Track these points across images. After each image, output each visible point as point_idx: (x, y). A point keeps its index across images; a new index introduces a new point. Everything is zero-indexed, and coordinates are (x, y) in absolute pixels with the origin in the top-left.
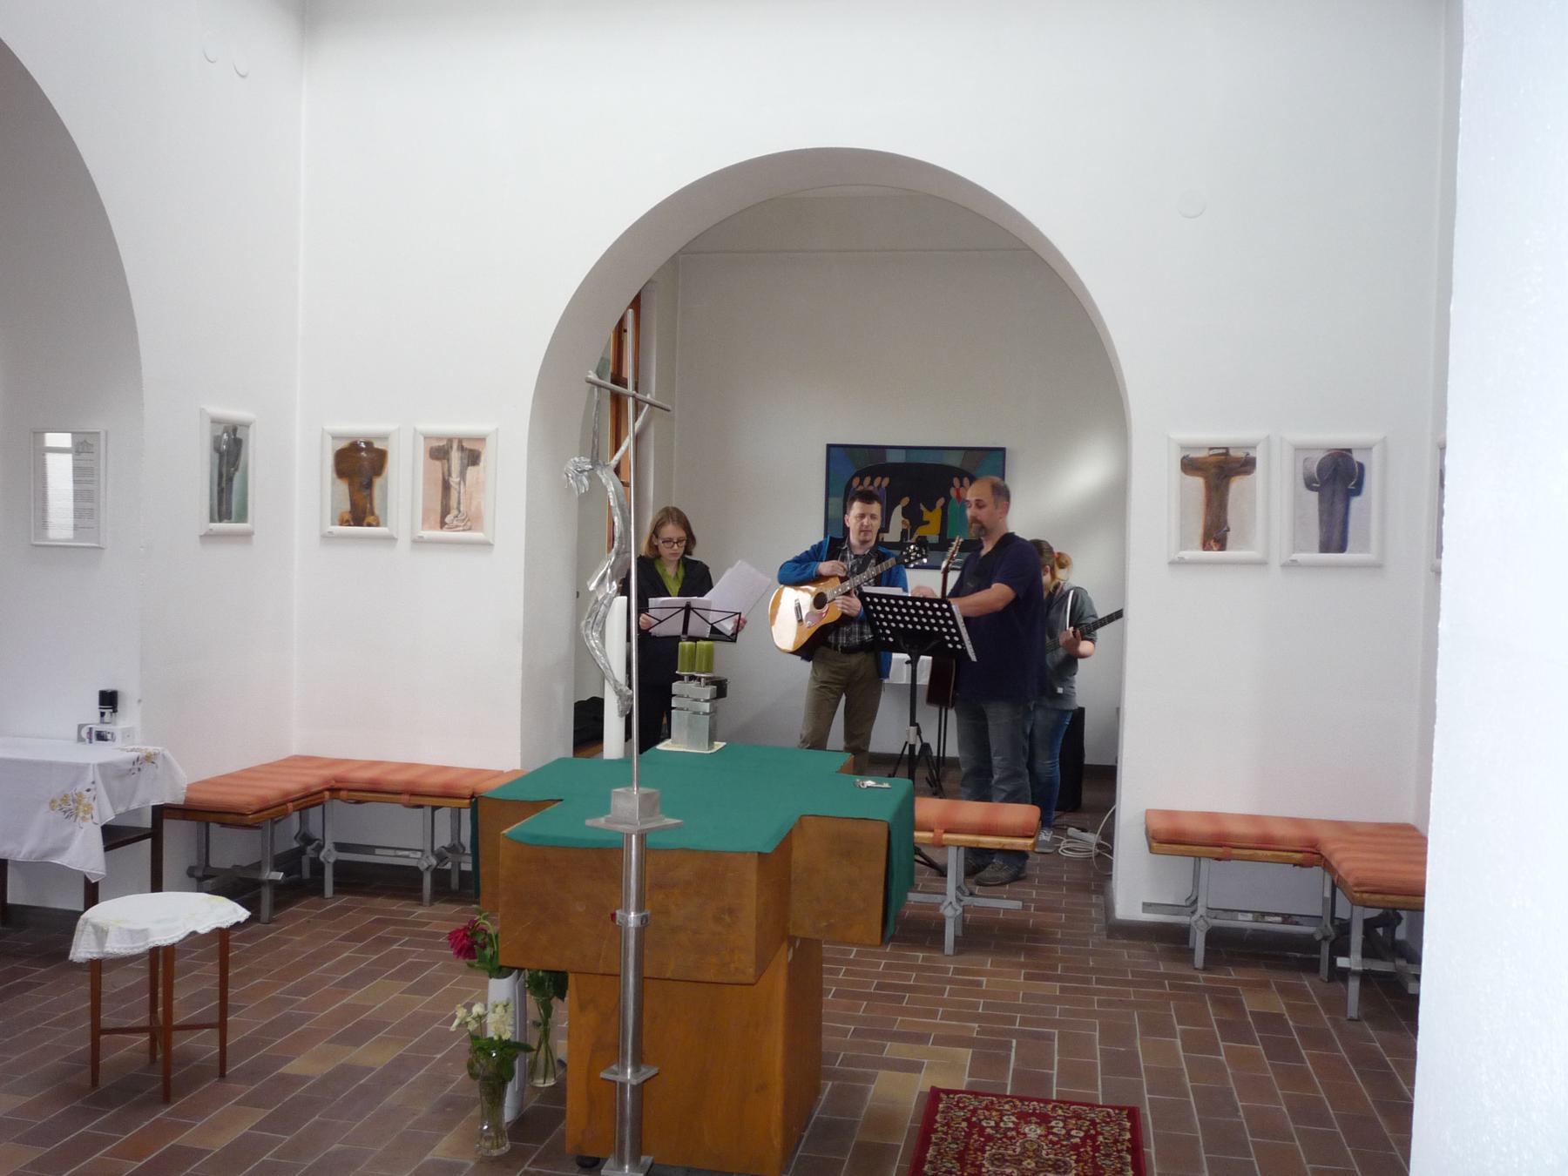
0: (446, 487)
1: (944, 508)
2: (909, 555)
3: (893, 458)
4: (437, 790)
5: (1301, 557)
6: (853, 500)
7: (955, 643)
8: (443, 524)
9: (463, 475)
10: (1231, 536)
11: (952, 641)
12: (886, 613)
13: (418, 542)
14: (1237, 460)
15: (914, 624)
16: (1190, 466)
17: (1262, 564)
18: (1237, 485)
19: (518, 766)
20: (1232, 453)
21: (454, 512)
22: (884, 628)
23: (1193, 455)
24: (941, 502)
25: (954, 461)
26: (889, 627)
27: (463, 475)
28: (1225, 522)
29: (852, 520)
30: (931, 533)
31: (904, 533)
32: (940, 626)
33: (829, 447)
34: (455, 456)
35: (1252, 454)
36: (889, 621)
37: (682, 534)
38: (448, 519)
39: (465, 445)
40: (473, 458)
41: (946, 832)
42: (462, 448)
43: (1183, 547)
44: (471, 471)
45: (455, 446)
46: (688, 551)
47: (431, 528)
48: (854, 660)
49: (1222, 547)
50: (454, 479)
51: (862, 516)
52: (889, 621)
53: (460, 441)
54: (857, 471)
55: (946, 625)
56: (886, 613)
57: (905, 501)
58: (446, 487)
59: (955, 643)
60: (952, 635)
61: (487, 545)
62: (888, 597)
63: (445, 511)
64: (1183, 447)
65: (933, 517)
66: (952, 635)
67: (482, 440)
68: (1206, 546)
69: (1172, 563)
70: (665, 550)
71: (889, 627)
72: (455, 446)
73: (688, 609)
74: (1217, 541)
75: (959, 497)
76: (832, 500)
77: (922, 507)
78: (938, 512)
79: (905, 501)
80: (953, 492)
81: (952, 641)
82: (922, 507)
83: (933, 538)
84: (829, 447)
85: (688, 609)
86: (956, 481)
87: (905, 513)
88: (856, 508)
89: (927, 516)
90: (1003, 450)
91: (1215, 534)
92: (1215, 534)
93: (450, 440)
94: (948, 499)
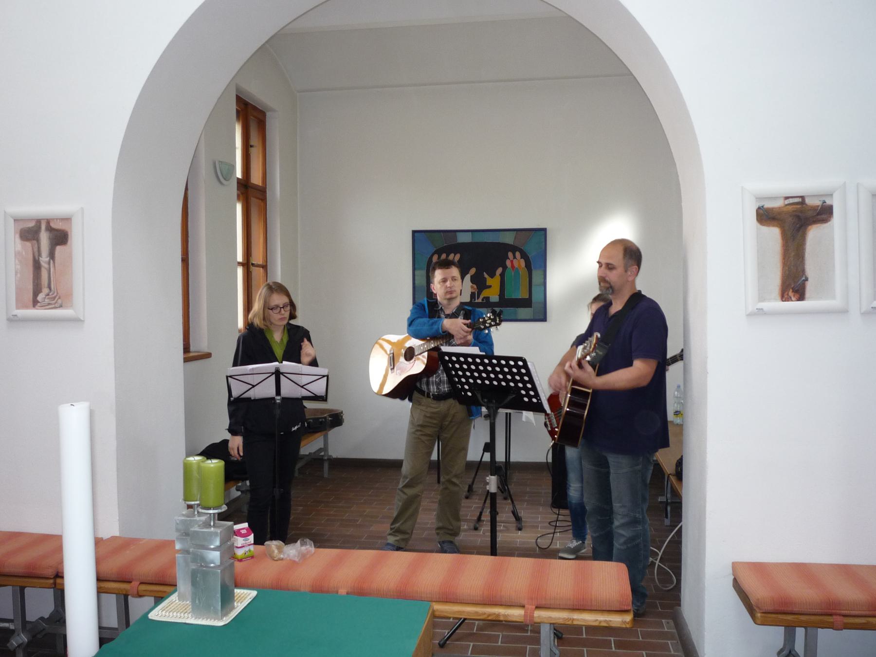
0: (37, 266)
1: (502, 275)
2: (485, 322)
3: (463, 239)
4: (20, 570)
5: (766, 305)
6: (434, 269)
7: (530, 397)
8: (35, 303)
9: (52, 255)
10: (809, 286)
11: (527, 395)
12: (464, 371)
13: (13, 320)
14: (814, 208)
15: (491, 380)
16: (765, 216)
17: (843, 312)
18: (814, 233)
19: (117, 534)
20: (808, 201)
21: (45, 291)
22: (463, 384)
23: (768, 205)
24: (499, 271)
25: (509, 239)
26: (467, 383)
27: (52, 255)
28: (803, 271)
29: (437, 287)
30: (493, 295)
31: (473, 295)
32: (516, 382)
33: (414, 232)
34: (44, 238)
35: (828, 202)
36: (467, 378)
37: (285, 300)
38: (40, 297)
39: (53, 225)
40: (60, 238)
41: (538, 607)
42: (49, 229)
43: (762, 299)
44: (59, 249)
45: (43, 227)
46: (293, 316)
47: (26, 307)
48: (443, 406)
49: (801, 297)
50: (44, 259)
51: (444, 280)
52: (467, 378)
53: (48, 222)
54: (436, 249)
55: (522, 381)
56: (464, 371)
57: (473, 271)
58: (37, 266)
59: (530, 397)
60: (527, 390)
61: (77, 321)
62: (466, 356)
63: (37, 291)
64: (759, 199)
65: (494, 282)
66: (527, 390)
67: (68, 220)
68: (784, 297)
69: (750, 315)
70: (275, 316)
71: (467, 383)
72: (43, 227)
73: (278, 374)
74: (796, 291)
75: (513, 266)
76: (417, 272)
77: (486, 276)
78: (497, 278)
79: (473, 271)
80: (508, 263)
81: (527, 395)
82: (486, 276)
83: (495, 298)
84: (414, 232)
85: (278, 374)
86: (510, 255)
87: (473, 280)
88: (438, 275)
89: (489, 281)
90: (544, 230)
91: (794, 285)
92: (794, 285)
93: (39, 222)
94: (505, 268)
